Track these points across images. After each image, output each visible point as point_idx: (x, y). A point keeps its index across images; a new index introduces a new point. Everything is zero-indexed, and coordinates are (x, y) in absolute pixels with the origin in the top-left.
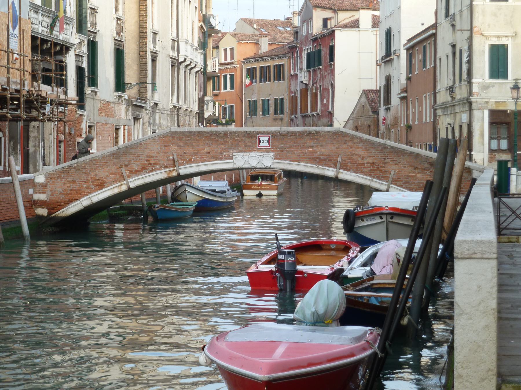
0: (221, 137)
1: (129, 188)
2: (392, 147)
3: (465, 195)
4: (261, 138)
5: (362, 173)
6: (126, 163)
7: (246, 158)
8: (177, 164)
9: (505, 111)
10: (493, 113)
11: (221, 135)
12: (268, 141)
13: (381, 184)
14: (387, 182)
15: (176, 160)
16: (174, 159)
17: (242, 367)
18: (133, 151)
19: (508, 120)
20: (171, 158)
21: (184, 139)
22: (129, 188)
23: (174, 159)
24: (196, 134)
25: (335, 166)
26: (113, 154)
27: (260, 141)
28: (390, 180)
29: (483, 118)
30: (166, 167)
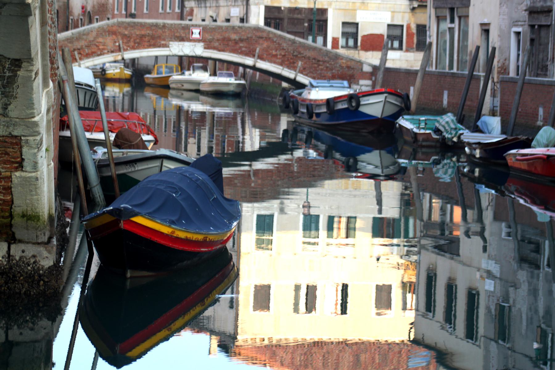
0: (160, 28)
1: (295, 79)
2: (300, 43)
3: (278, 81)
4: (194, 31)
5: (275, 63)
6: (79, 47)
7: (181, 46)
8: (122, 50)
9: (279, 8)
10: (268, 9)
11: (160, 27)
12: (200, 33)
13: (290, 73)
14: (295, 71)
15: (121, 46)
16: (119, 45)
17: (278, 224)
18: (85, 37)
19: (281, 16)
20: (117, 44)
21: (129, 29)
22: (295, 79)
23: (119, 45)
24: (139, 25)
25: (254, 56)
26: (68, 39)
27: (192, 33)
28: (298, 70)
29: (259, 13)
30: (112, 52)
